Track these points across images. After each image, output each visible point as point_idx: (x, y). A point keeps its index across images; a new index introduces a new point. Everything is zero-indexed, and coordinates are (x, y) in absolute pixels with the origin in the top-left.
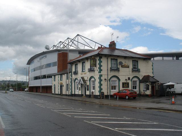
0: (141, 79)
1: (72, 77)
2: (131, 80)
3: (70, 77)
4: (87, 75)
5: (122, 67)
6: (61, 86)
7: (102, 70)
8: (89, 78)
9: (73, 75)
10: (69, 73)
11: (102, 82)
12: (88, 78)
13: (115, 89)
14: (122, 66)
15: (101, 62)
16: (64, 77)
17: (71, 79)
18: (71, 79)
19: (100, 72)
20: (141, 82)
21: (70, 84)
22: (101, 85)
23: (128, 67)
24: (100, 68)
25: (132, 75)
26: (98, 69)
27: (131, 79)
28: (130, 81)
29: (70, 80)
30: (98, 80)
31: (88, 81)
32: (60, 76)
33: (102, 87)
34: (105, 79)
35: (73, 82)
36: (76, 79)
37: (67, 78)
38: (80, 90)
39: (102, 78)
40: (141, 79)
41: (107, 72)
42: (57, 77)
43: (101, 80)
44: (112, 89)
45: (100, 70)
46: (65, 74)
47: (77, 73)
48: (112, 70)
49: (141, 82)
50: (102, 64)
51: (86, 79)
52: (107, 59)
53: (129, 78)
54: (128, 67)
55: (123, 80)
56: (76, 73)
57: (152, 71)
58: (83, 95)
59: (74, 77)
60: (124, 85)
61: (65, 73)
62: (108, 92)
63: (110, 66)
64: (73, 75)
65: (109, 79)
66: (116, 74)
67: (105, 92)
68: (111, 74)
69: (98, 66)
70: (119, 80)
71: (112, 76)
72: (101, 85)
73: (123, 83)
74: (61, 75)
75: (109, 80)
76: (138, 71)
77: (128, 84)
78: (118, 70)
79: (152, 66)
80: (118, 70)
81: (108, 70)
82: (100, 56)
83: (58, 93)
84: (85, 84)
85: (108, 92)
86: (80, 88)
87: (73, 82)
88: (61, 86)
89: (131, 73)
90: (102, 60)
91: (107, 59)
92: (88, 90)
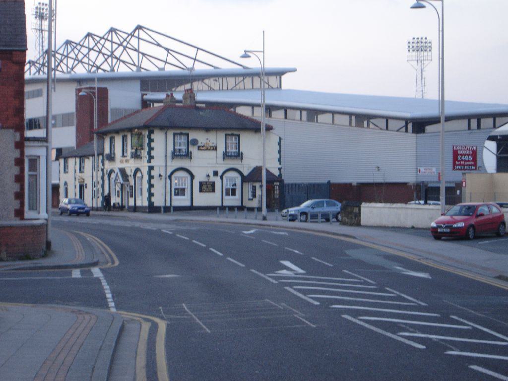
0: (246, 173)
1: (103, 165)
2: (222, 177)
3: (101, 165)
4: (130, 165)
5: (199, 148)
6: (82, 187)
7: (153, 157)
8: (133, 172)
9: (107, 162)
10: (98, 155)
11: (153, 181)
12: (131, 171)
13: (183, 194)
14: (199, 147)
15: (151, 140)
16: (88, 163)
17: (103, 170)
18: (103, 170)
19: (149, 161)
20: (246, 182)
21: (101, 182)
22: (151, 186)
23: (214, 150)
24: (149, 153)
25: (224, 166)
26: (146, 154)
27: (220, 174)
28: (219, 177)
29: (100, 174)
30: (146, 177)
31: (133, 178)
32: (78, 160)
33: (153, 190)
34: (160, 175)
35: (106, 177)
36: (112, 171)
37: (94, 168)
38: (118, 196)
39: (153, 173)
40: (246, 173)
41: (164, 161)
42: (71, 161)
43: (151, 177)
44: (175, 195)
45: (151, 157)
46: (91, 158)
47: (113, 157)
48: (175, 155)
49: (245, 179)
50: (153, 145)
51: (128, 172)
52: (166, 133)
53: (216, 173)
54: (215, 149)
55: (200, 177)
56: (111, 158)
57: (278, 156)
58: (125, 207)
59: (108, 166)
60: (204, 187)
61: (90, 155)
62: (166, 200)
63: (170, 149)
64: (107, 162)
65: (168, 173)
66: (186, 165)
67: (158, 201)
68: (173, 165)
69: (147, 149)
70: (192, 177)
71: (174, 168)
72: (151, 186)
73: (201, 184)
74: (82, 158)
75: (170, 177)
76: (239, 155)
77: (213, 184)
78: (188, 155)
79: (279, 144)
80: (188, 155)
81: (166, 156)
82: (151, 129)
83: (229, 79)
84: (127, 183)
85: (166, 200)
86: (118, 192)
87: (106, 177)
88: (82, 187)
89: (220, 160)
90: (153, 136)
91: (166, 133)
92: (131, 196)
